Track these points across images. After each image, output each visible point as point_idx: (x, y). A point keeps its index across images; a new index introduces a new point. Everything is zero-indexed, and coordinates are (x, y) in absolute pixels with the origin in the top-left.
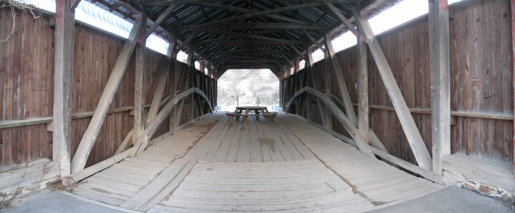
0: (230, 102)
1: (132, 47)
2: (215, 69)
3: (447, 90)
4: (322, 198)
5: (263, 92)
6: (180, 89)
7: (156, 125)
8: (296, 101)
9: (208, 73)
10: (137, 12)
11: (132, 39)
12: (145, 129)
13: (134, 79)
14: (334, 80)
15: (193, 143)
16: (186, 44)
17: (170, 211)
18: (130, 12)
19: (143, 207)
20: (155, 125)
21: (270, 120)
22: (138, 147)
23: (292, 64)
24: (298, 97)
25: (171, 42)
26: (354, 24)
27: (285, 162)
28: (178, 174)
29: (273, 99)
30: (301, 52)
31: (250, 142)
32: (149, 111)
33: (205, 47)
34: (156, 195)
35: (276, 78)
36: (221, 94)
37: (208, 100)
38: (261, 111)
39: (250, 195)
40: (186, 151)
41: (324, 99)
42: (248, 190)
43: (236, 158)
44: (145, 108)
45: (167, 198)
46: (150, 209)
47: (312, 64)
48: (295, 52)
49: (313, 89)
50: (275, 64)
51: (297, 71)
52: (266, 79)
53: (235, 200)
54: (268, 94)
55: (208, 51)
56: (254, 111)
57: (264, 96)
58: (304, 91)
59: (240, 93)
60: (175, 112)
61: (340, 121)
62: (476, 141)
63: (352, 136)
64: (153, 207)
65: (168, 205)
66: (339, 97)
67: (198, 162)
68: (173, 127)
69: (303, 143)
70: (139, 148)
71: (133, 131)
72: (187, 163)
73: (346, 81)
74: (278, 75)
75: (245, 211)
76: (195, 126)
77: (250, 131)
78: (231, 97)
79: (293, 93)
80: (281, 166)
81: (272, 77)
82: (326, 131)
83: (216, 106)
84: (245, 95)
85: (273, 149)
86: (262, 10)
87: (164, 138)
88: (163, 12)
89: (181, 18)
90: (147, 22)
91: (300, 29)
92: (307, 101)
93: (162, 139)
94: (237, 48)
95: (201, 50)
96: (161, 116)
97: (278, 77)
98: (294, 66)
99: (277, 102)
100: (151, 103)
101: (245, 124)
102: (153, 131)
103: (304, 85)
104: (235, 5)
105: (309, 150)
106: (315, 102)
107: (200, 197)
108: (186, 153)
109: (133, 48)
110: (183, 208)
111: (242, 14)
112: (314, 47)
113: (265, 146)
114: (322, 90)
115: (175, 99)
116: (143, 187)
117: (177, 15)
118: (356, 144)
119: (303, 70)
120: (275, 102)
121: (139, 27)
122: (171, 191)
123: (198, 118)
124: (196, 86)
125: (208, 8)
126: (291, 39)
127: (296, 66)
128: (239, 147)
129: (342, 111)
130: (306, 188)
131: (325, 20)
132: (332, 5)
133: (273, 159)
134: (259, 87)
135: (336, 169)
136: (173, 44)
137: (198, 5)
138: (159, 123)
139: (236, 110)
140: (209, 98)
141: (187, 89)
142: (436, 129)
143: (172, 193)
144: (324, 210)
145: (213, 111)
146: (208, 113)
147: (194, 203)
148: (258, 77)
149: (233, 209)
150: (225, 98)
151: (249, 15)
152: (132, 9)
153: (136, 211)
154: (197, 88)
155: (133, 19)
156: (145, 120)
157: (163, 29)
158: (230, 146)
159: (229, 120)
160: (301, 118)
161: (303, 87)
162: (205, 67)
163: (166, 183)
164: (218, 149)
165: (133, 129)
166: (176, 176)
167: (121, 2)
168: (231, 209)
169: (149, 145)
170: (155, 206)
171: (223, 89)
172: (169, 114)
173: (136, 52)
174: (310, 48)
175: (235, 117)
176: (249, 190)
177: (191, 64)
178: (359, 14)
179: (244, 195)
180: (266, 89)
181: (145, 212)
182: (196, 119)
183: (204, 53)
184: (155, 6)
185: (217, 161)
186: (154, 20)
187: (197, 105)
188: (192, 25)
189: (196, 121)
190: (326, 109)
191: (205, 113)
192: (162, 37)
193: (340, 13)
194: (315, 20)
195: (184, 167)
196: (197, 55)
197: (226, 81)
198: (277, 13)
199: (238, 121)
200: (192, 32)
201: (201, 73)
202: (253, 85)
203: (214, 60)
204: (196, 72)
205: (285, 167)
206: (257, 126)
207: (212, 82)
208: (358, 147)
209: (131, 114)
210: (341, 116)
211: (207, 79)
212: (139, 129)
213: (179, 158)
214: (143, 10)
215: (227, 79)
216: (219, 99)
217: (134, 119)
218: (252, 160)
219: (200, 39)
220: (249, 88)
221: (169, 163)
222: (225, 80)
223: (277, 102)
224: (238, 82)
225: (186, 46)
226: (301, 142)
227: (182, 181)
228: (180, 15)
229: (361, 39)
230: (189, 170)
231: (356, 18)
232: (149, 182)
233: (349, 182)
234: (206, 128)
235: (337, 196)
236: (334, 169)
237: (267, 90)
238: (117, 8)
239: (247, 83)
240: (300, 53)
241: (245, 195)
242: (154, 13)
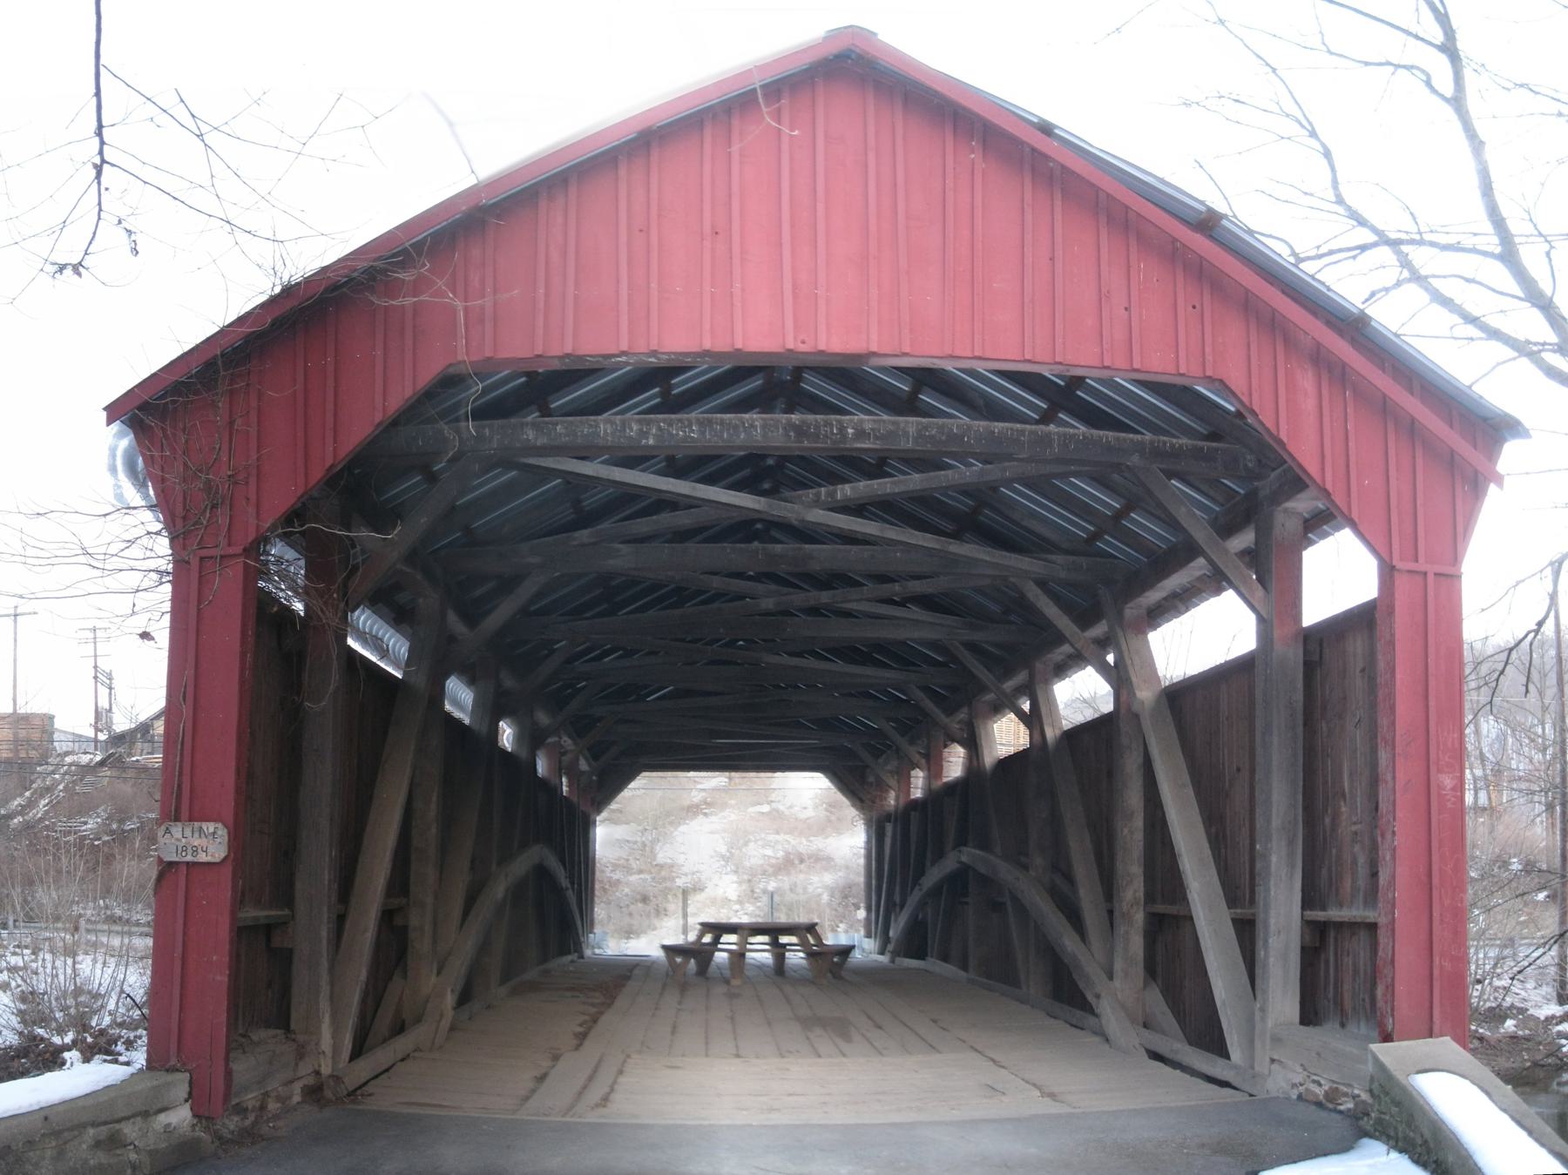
3: (1291, 855)
14: (1055, 823)
24: (936, 892)
29: (836, 910)
35: (849, 811)
38: (794, 939)
49: (992, 857)
51: (937, 784)
58: (958, 865)
62: (1357, 987)
74: (861, 801)
78: (638, 897)
79: (921, 872)
84: (702, 890)
92: (967, 903)
97: (857, 809)
99: (851, 926)
103: (961, 842)
106: (998, 907)
113: (818, 1031)
120: (842, 927)
126: (914, 664)
127: (934, 764)
132: (1034, 587)
134: (769, 852)
142: (1262, 953)
148: (765, 808)
178: (1120, 613)
180: (802, 861)
201: (547, 788)
202: (741, 842)
209: (277, 942)
210: (1069, 942)
220: (723, 857)
223: (851, 926)
229: (1037, 737)
231: (1111, 628)
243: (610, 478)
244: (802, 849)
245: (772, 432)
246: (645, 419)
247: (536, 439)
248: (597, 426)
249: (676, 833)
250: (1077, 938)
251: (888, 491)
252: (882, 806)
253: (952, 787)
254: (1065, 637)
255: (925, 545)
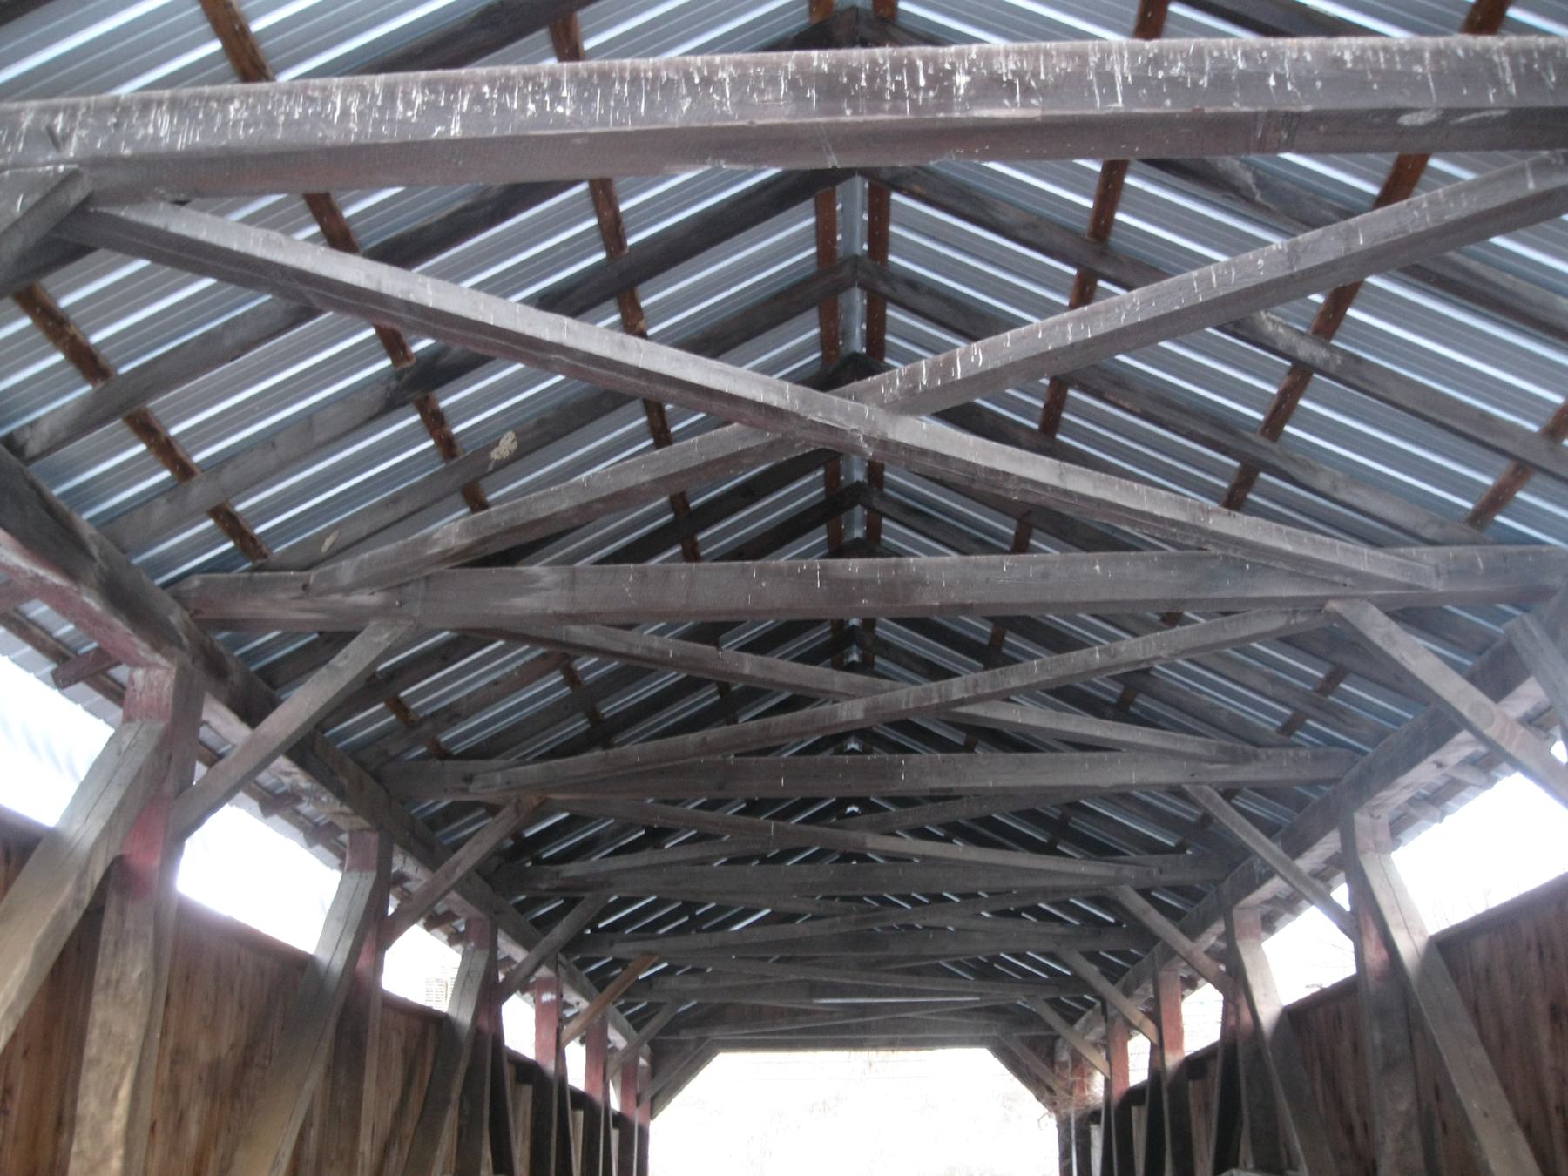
1: (79, 888)
2: (633, 1051)
9: (588, 1076)
10: (142, 654)
11: (86, 832)
13: (67, 1115)
16: (454, 887)
18: (95, 645)
23: (1134, 1009)
25: (349, 869)
26: (1540, 727)
30: (1193, 932)
33: (571, 904)
47: (1268, 1012)
48: (1148, 938)
50: (1029, 1019)
51: (1172, 1060)
55: (595, 930)
73: (1528, 1129)
86: (937, 673)
88: (314, 667)
89: (429, 712)
90: (206, 723)
91: (1179, 786)
94: (781, 918)
95: (545, 924)
98: (1150, 1026)
104: (759, 646)
109: (87, 897)
111: (797, 701)
112: (1274, 900)
117: (403, 694)
121: (139, 758)
125: (595, 659)
131: (1335, 715)
132: (1382, 619)
136: (368, 880)
137: (536, 641)
151: (852, 711)
152: (110, 627)
155: (116, 693)
157: (302, 781)
162: (572, 1038)
167: (41, 572)
173: (105, 925)
174: (1252, 908)
177: (475, 1017)
183: (569, 947)
184: (264, 625)
186: (251, 711)
188: (496, 762)
192: (294, 830)
193: (1443, 664)
194: (1268, 724)
196: (519, 954)
198: (1029, 691)
200: (493, 810)
203: (636, 989)
204: (508, 1072)
207: (615, 1134)
211: (580, 1114)
214: (185, 641)
219: (545, 856)
225: (454, 895)
228: (422, 694)
238: (16, 610)
240: (1181, 942)
242: (254, 668)
243: (412, 298)
245: (762, 92)
246: (443, 80)
247: (174, 134)
248: (326, 99)
251: (1070, 339)
252: (1085, 1098)
253: (1197, 1064)
254: (1459, 715)
255: (1157, 512)
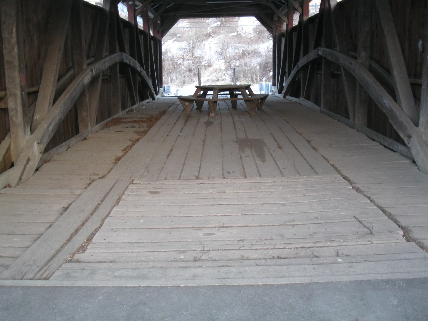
0: (186, 79)
4: (348, 244)
5: (243, 60)
6: (94, 56)
7: (53, 124)
8: (301, 74)
12: (32, 133)
15: (123, 151)
17: (89, 269)
19: (42, 271)
20: (51, 123)
21: (257, 108)
22: (22, 167)
24: (305, 67)
27: (283, 178)
28: (99, 204)
29: (262, 73)
31: (222, 145)
32: (36, 99)
34: (63, 247)
35: (267, 34)
36: (169, 64)
37: (146, 75)
38: (240, 93)
39: (223, 233)
40: (112, 166)
41: (354, 71)
42: (220, 225)
43: (199, 172)
44: (29, 94)
45: (82, 249)
46: (54, 272)
49: (335, 52)
51: (305, 18)
52: (249, 37)
53: (199, 242)
54: (252, 65)
56: (228, 92)
57: (246, 68)
58: (317, 57)
59: (203, 63)
60: (87, 99)
61: (384, 111)
63: (406, 140)
64: (60, 267)
65: (86, 261)
66: (383, 67)
67: (133, 181)
68: (86, 126)
69: (313, 148)
70: (24, 169)
71: (11, 138)
72: (113, 186)
74: (272, 28)
75: (216, 261)
76: (125, 122)
77: (221, 127)
79: (297, 60)
80: (276, 183)
81: (260, 33)
82: (354, 129)
83: (161, 87)
84: (211, 66)
85: (262, 156)
87: (71, 146)
92: (321, 74)
93: (67, 149)
96: (61, 107)
98: (300, 9)
99: (268, 79)
100: (40, 84)
101: (212, 115)
102: (48, 134)
103: (317, 45)
105: (325, 159)
106: (335, 76)
107: (140, 241)
108: (112, 169)
110: (111, 262)
113: (248, 151)
114: (351, 53)
115: (84, 75)
116: (39, 235)
118: (411, 154)
119: (316, 16)
120: (264, 79)
122: (89, 235)
123: (129, 109)
124: (122, 50)
128: (202, 153)
129: (389, 93)
130: (320, 223)
133: (261, 173)
134: (237, 51)
135: (372, 195)
138: (57, 119)
139: (197, 92)
140: (147, 73)
141: (106, 56)
143: (92, 239)
144: (352, 264)
145: (157, 94)
146: (147, 98)
147: (130, 251)
148: (235, 34)
149: (195, 258)
150: (176, 72)
153: (30, 279)
154: (124, 54)
156: (30, 116)
158: (187, 154)
159: (184, 109)
160: (309, 104)
161: (315, 48)
162: (137, 15)
163: (80, 223)
164: (167, 158)
165: (9, 134)
166: (96, 209)
168: (192, 258)
169: (43, 162)
170: (63, 266)
171: (173, 56)
172: (76, 101)
175: (195, 104)
176: (222, 226)
177: (110, 8)
179: (213, 234)
180: (249, 54)
181: (47, 278)
182: (127, 109)
185: (166, 179)
187: (127, 85)
189: (127, 113)
190: (358, 88)
191: (142, 99)
195: (108, 192)
197: (178, 41)
199: (201, 112)
202: (226, 47)
205: (283, 186)
206: (233, 119)
207: (152, 42)
208: (416, 160)
211: (142, 36)
212: (21, 133)
213: (99, 178)
215: (178, 37)
216: (166, 75)
217: (8, 116)
218: (226, 175)
221: (83, 189)
222: (174, 41)
224: (198, 43)
226: (309, 144)
227: (108, 216)
230: (118, 197)
232: (48, 225)
233: (397, 220)
234: (145, 125)
235: (375, 243)
236: (369, 195)
237: (252, 57)
239: (215, 44)
241: (215, 233)
244: (249, 49)
249: (201, 45)
250: (391, 98)
252: (281, 30)
